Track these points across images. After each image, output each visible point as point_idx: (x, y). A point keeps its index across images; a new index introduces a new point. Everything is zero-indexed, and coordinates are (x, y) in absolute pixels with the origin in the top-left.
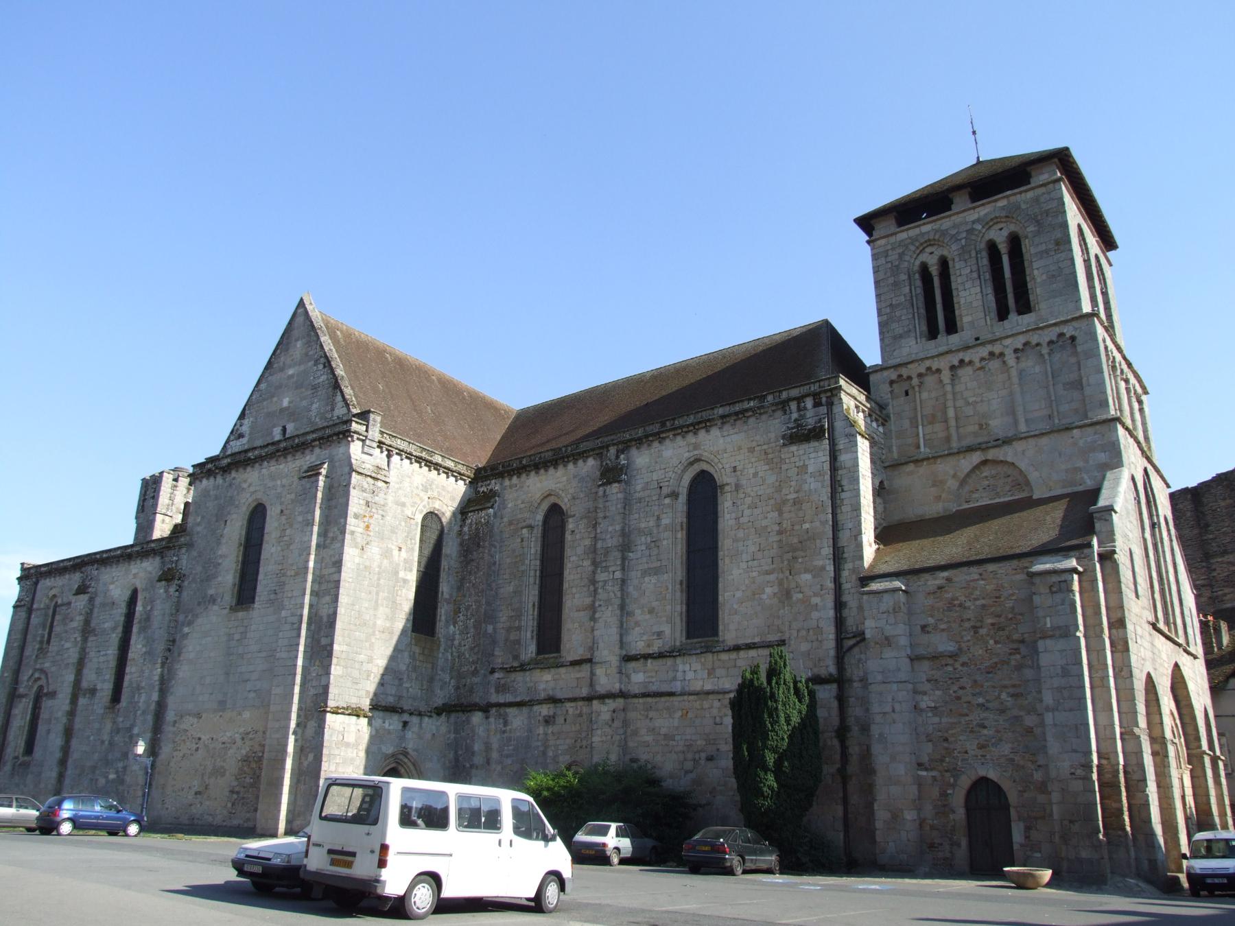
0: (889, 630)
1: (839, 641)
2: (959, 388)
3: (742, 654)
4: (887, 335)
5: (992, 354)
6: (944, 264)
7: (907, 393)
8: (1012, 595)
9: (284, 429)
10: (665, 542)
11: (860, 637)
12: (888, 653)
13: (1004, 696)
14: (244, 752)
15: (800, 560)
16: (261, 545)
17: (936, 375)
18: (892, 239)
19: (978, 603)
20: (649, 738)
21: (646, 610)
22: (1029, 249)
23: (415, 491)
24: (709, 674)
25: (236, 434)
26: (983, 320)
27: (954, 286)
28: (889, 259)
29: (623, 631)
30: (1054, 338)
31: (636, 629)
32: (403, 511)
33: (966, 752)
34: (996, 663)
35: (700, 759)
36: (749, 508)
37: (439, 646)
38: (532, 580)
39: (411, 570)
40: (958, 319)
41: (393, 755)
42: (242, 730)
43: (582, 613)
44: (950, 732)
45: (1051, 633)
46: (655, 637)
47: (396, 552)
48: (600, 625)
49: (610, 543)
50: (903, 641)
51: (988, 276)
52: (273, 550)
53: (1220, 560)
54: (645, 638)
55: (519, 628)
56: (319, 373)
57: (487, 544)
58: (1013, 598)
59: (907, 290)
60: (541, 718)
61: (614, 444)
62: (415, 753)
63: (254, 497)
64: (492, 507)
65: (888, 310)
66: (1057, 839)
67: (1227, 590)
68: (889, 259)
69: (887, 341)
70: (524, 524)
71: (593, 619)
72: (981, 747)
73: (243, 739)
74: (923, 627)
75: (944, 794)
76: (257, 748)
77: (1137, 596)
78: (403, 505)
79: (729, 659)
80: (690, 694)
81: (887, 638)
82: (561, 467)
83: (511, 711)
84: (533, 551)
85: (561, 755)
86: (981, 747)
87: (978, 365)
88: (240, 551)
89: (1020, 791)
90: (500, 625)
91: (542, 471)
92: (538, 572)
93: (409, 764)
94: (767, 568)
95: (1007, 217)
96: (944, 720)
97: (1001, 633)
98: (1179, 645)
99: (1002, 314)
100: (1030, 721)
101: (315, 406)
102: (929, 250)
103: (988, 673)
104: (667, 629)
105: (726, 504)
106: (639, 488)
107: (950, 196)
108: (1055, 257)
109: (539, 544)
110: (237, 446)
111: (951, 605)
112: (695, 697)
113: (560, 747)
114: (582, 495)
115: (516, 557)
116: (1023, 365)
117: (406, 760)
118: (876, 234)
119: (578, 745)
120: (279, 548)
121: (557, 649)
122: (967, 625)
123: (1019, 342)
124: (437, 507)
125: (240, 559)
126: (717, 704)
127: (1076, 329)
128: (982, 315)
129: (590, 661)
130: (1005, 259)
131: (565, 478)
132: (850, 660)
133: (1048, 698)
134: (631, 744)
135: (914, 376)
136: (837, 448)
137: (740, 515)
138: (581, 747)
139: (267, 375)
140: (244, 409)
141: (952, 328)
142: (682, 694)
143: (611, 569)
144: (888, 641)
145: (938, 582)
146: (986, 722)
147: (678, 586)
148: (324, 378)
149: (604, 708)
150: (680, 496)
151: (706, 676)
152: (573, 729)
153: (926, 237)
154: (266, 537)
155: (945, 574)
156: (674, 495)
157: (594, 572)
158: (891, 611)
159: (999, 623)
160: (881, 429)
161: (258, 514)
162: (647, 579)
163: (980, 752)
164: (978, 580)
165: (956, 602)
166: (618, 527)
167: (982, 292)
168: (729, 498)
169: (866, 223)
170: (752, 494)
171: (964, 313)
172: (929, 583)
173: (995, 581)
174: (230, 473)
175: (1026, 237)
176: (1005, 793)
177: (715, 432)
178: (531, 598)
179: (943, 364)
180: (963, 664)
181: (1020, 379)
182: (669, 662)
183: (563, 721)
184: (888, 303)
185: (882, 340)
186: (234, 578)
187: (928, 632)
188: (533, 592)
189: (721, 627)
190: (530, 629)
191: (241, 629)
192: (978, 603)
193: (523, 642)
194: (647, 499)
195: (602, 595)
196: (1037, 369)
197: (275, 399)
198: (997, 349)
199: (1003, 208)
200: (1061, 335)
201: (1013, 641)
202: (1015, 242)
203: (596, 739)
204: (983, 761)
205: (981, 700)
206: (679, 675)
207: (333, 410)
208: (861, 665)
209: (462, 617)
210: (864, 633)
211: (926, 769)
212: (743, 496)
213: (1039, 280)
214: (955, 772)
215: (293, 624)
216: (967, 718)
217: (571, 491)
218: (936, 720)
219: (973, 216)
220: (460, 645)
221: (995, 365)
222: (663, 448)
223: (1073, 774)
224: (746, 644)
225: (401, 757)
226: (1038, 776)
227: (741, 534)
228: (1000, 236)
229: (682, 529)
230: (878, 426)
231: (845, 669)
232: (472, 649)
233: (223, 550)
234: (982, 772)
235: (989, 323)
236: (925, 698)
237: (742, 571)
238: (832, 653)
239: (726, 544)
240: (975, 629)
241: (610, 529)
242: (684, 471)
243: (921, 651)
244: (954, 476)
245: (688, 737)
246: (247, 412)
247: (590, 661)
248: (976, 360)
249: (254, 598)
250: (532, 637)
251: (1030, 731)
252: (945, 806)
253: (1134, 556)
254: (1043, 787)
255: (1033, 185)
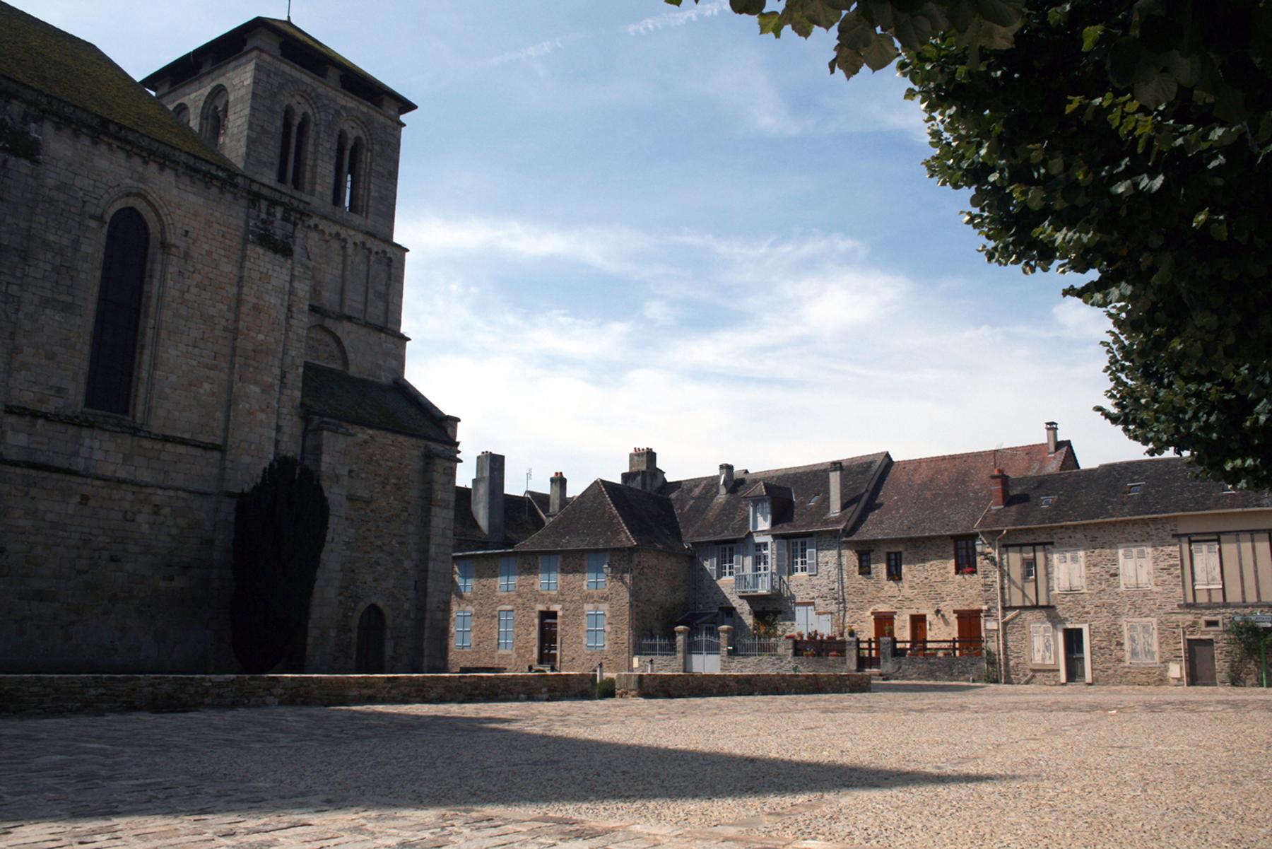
3: (169, 446)
5: (338, 235)
8: (410, 465)
15: (251, 369)
24: (125, 460)
30: (388, 255)
31: (23, 373)
34: (393, 515)
35: (100, 558)
36: (197, 286)
46: (52, 393)
61: (25, 101)
72: (375, 580)
79: (153, 448)
80: (97, 478)
86: (375, 580)
95: (363, 122)
103: (388, 522)
112: (103, 482)
122: (378, 479)
126: (130, 496)
137: (186, 289)
142: (87, 476)
145: (365, 437)
151: (120, 461)
162: (48, 311)
180: (372, 511)
182: (72, 431)
204: (618, 598)
205: (379, 543)
212: (192, 269)
224: (164, 435)
234: (374, 601)
240: (384, 484)
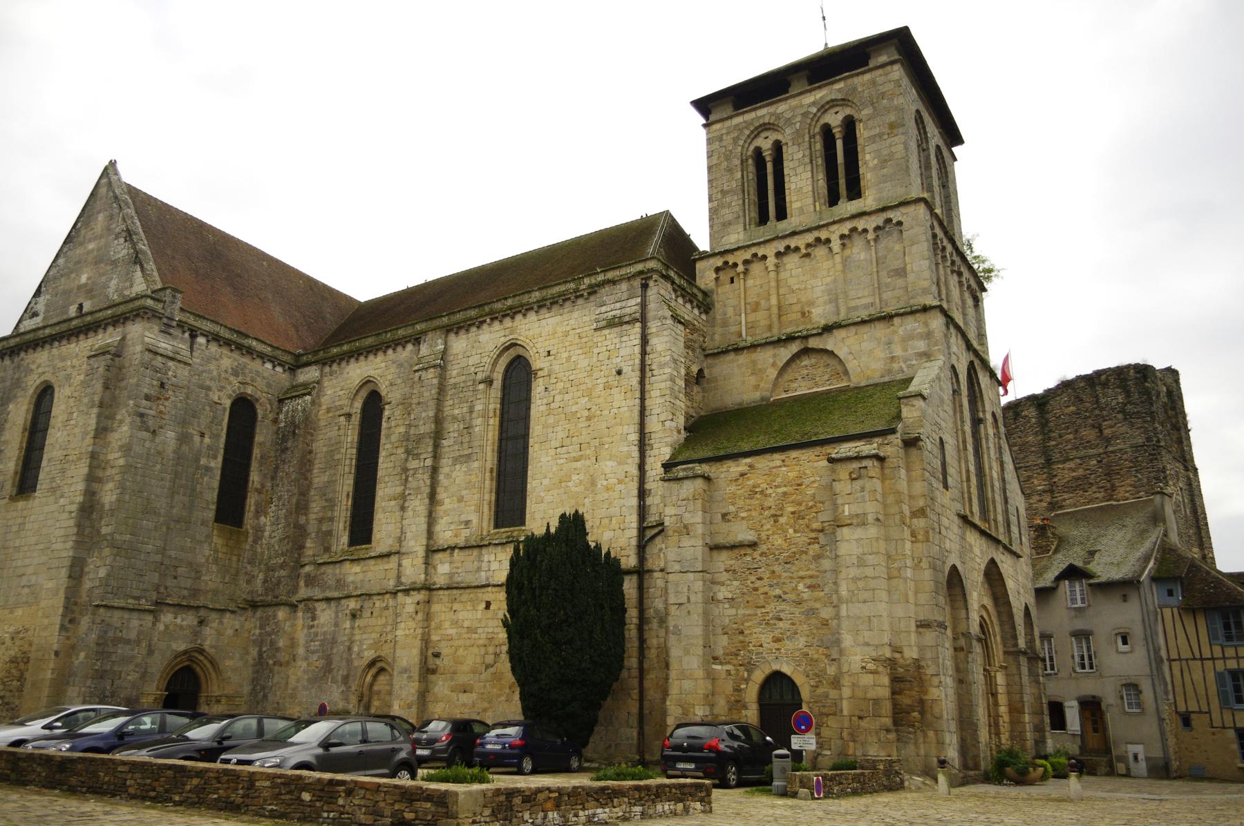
0: (688, 518)
1: (642, 530)
2: (782, 275)
4: (715, 220)
6: (778, 147)
7: (732, 281)
8: (814, 482)
9: (81, 307)
10: (477, 429)
11: (660, 527)
12: (686, 542)
13: (801, 587)
14: (12, 653)
15: (606, 446)
16: (46, 429)
17: (762, 263)
18: (728, 123)
19: (780, 490)
20: (452, 632)
21: (455, 498)
22: (862, 132)
23: (223, 375)
25: (30, 312)
26: (812, 206)
27: (786, 171)
28: (724, 143)
29: (431, 520)
32: (207, 395)
33: (761, 646)
36: (560, 393)
37: (247, 537)
38: (347, 469)
39: (215, 457)
40: (788, 205)
41: (185, 652)
42: (12, 629)
43: (393, 503)
44: (746, 624)
45: (849, 522)
46: (463, 526)
47: (197, 439)
48: (409, 513)
49: (422, 430)
50: (700, 529)
51: (820, 161)
52: (59, 434)
53: (1061, 466)
54: (452, 527)
55: (331, 519)
56: (119, 248)
57: (302, 432)
58: (815, 485)
59: (739, 175)
60: (348, 612)
62: (213, 650)
63: (42, 379)
64: (309, 394)
65: (719, 196)
66: (845, 734)
67: (1066, 496)
68: (724, 143)
69: (716, 228)
70: (342, 412)
71: (403, 508)
72: (777, 640)
73: (13, 639)
74: (724, 516)
75: (737, 690)
76: (26, 648)
77: (946, 487)
78: (209, 389)
81: (686, 527)
82: (380, 354)
83: (320, 606)
84: (349, 439)
85: (366, 649)
86: (777, 640)
87: (804, 251)
88: (23, 436)
89: (812, 686)
90: (312, 516)
91: (362, 358)
92: (354, 461)
93: (206, 662)
94: (574, 454)
96: (741, 612)
97: (801, 522)
98: (997, 541)
99: (833, 200)
100: (826, 613)
101: (114, 282)
102: (764, 135)
103: (786, 563)
104: (474, 518)
105: (538, 388)
106: (454, 373)
107: (789, 78)
108: (889, 141)
109: (357, 432)
110: (29, 324)
111: (753, 493)
113: (366, 642)
114: (399, 381)
115: (333, 445)
116: (847, 252)
117: (201, 658)
118: (712, 118)
119: (383, 639)
120: (65, 433)
121: (368, 540)
123: (845, 228)
124: (250, 392)
125: (24, 445)
127: (903, 214)
128: (810, 200)
129: (398, 553)
130: (839, 144)
131: (383, 364)
132: (652, 550)
133: (844, 591)
134: (434, 638)
135: (740, 263)
136: (649, 331)
138: (386, 642)
139: (65, 250)
140: (40, 286)
141: (782, 214)
143: (423, 456)
144: (686, 530)
146: (782, 615)
147: (488, 474)
148: (125, 252)
149: (409, 600)
150: (495, 382)
152: (379, 623)
153: (761, 121)
154: (52, 421)
155: (748, 460)
156: (489, 382)
157: (406, 460)
158: (691, 498)
159: (800, 512)
160: (704, 317)
161: (45, 394)
162: (458, 467)
163: (776, 645)
164: (780, 467)
165: (757, 490)
166: (431, 414)
167: (812, 177)
168: (541, 384)
169: (704, 105)
170: (564, 379)
171: (794, 198)
172: (731, 470)
173: (797, 468)
174: (18, 354)
175: (861, 121)
176: (797, 687)
177: (532, 316)
178: (345, 488)
179: (770, 251)
180: (762, 554)
181: (844, 266)
183: (369, 615)
184: (719, 189)
185: (711, 227)
186: (16, 465)
187: (729, 521)
188: (348, 482)
189: (528, 516)
190: (343, 519)
191: (20, 520)
192: (780, 490)
193: (334, 533)
194: (462, 385)
195: (412, 483)
196: (862, 256)
197: (73, 275)
198: (823, 235)
199: (839, 90)
200: (889, 221)
201: (813, 531)
202: (850, 125)
203: (399, 633)
205: (778, 592)
206: (484, 565)
207: (131, 286)
208: (662, 555)
209: (273, 508)
210: (663, 524)
211: (721, 664)
213: (871, 165)
214: (750, 666)
215: (71, 512)
216: (764, 610)
217: (390, 377)
218: (733, 611)
219: (809, 99)
220: (270, 537)
221: (820, 252)
222: (481, 332)
223: (863, 668)
225: (196, 655)
226: (831, 670)
227: (551, 420)
228: (834, 119)
229: (495, 416)
230: (700, 313)
231: (646, 559)
232: (281, 540)
233: (7, 436)
234: (776, 667)
235: (818, 208)
236: (723, 588)
237: (550, 458)
238: (634, 542)
239: (536, 430)
240: (775, 517)
241: (424, 415)
242: (499, 356)
243: (721, 540)
244: (774, 365)
245: (491, 630)
246: (43, 289)
247: (398, 553)
248: (802, 247)
249: (35, 487)
250: (345, 527)
251: (825, 623)
252: (738, 701)
253: (946, 446)
254: (836, 683)
255: (871, 65)
